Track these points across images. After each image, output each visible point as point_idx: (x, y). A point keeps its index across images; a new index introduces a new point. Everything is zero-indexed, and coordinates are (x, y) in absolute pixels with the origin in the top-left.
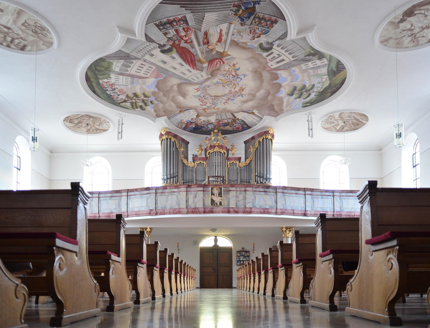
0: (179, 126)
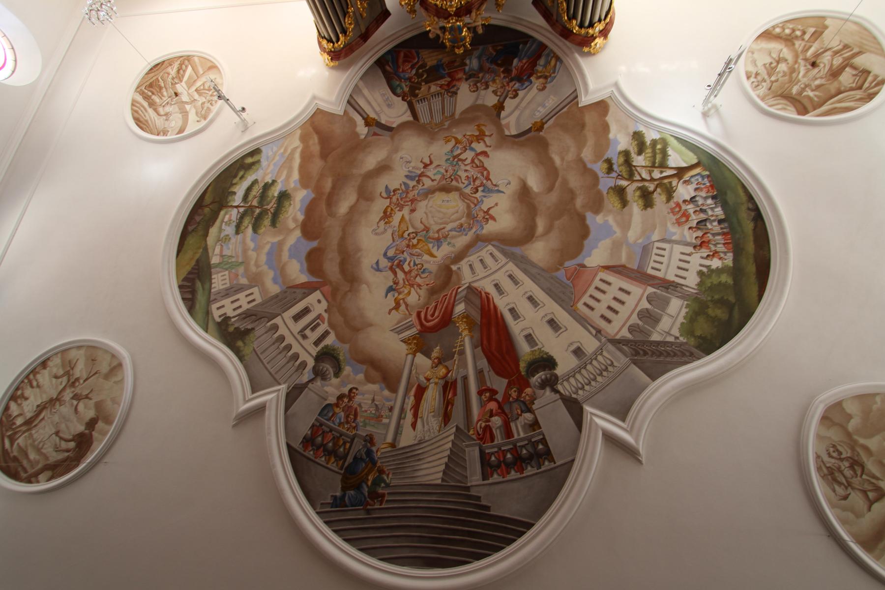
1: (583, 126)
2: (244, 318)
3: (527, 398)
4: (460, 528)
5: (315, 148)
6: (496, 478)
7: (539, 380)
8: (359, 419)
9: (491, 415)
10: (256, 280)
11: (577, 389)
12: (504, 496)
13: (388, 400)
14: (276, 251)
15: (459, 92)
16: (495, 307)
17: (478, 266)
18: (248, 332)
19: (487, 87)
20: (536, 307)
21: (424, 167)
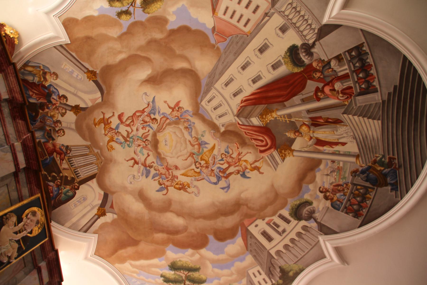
1: (88, 38)
2: (272, 275)
3: (320, 65)
4: (408, 104)
5: (130, 250)
6: (376, 83)
7: (307, 57)
8: (341, 182)
9: (334, 90)
10: (243, 273)
11: (311, 29)
12: (387, 76)
13: (327, 164)
14: (217, 264)
15: (66, 144)
16: (253, 94)
17: (220, 111)
18: (282, 270)
19: (59, 122)
20: (250, 63)
21: (138, 164)
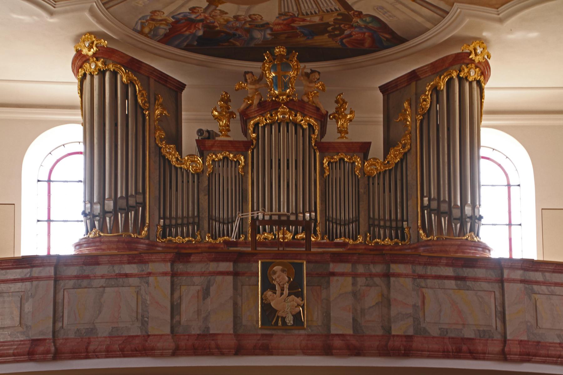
0: (146, 30)
15: (277, 15)
